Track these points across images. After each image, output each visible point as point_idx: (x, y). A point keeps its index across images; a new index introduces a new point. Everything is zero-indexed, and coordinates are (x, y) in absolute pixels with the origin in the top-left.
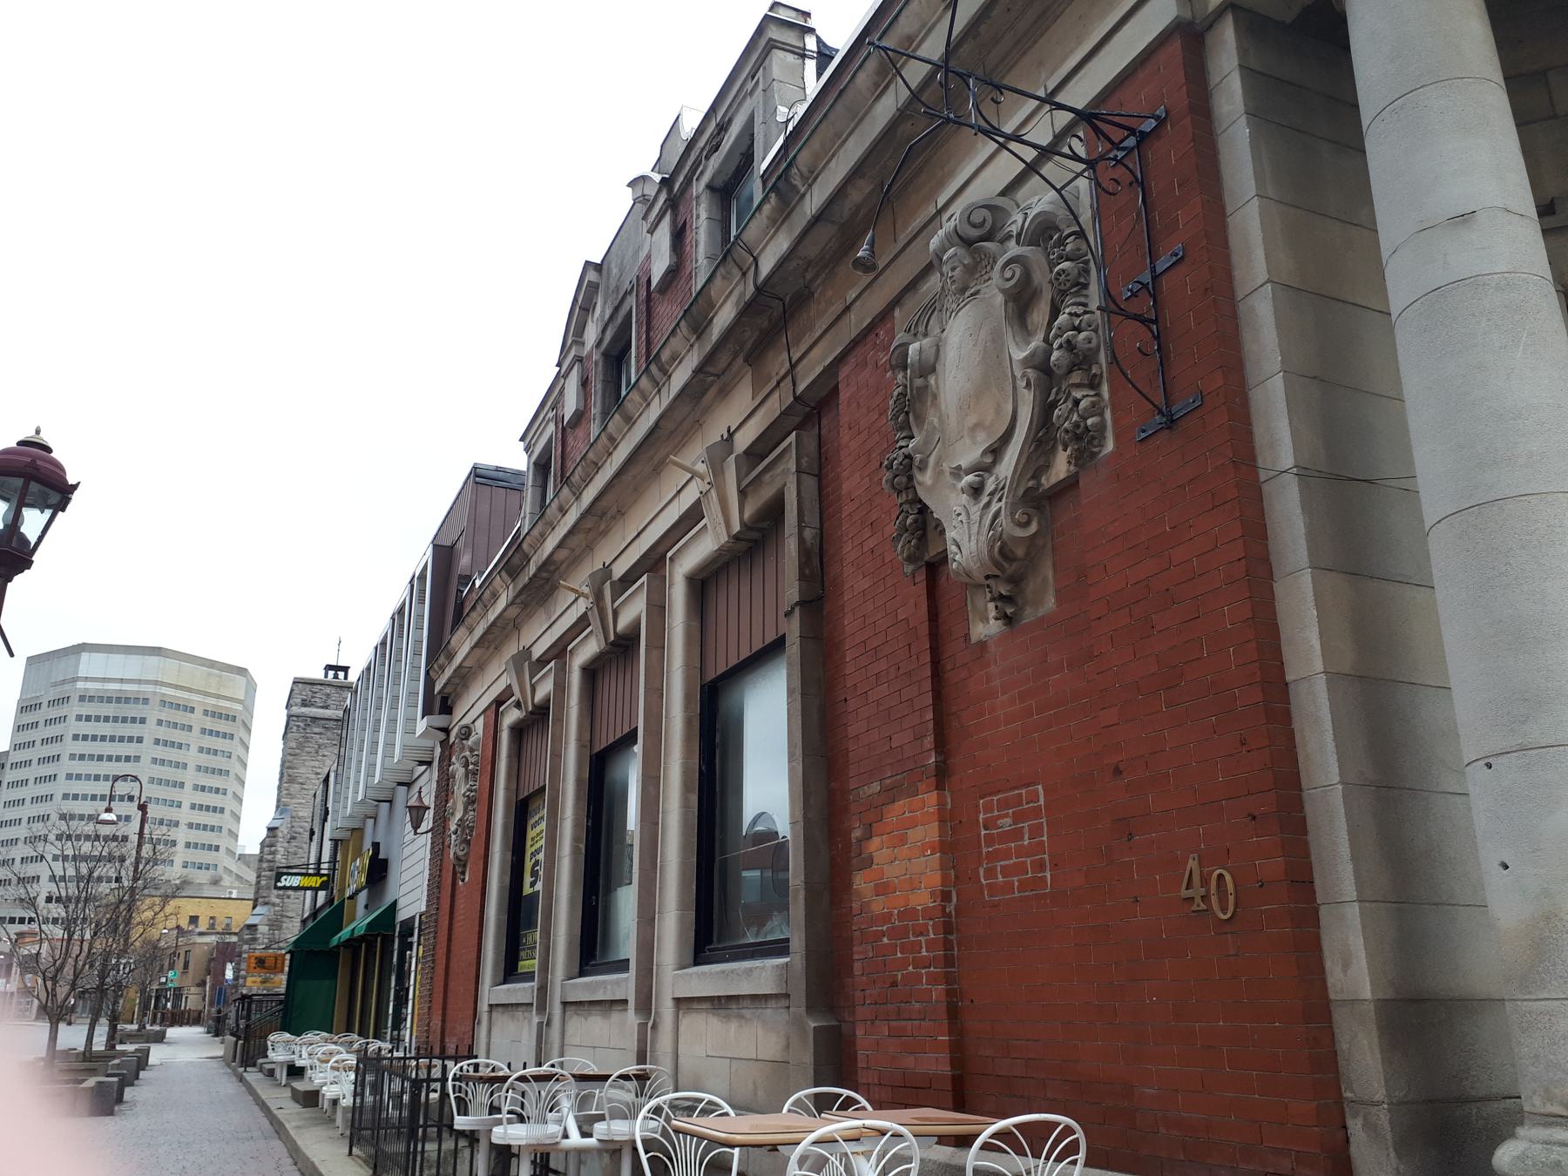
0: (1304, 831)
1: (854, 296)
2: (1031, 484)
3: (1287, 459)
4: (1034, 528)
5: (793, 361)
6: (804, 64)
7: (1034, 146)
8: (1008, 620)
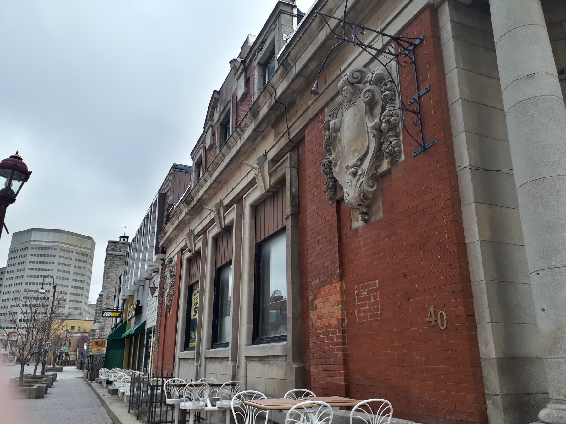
1: (311, 103)
2: (374, 172)
3: (466, 163)
4: (375, 187)
5: (289, 126)
6: (293, 19)
7: (376, 49)
8: (366, 221)
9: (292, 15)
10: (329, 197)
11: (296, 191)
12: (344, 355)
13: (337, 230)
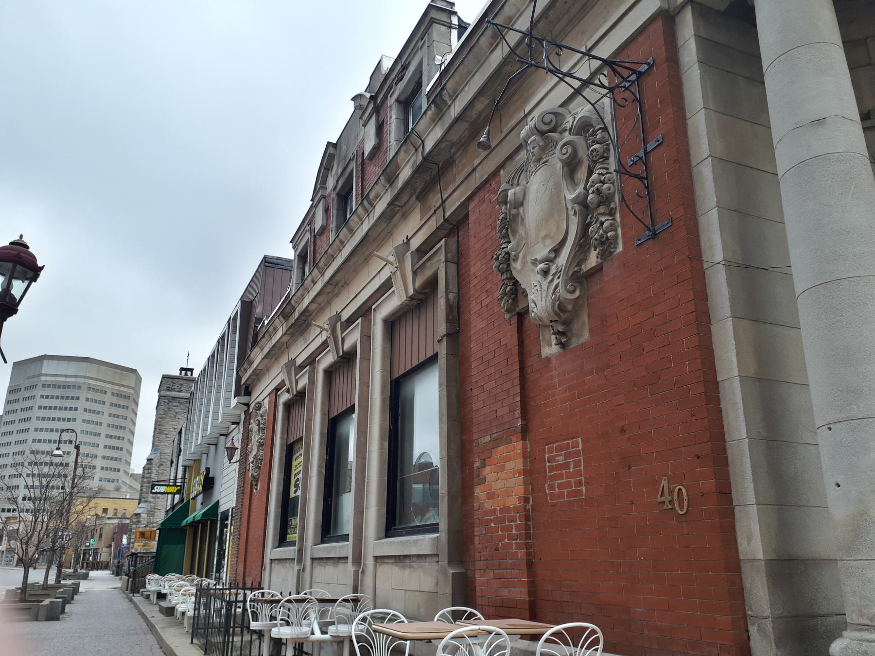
1: (478, 162)
2: (576, 269)
3: (719, 256)
4: (577, 294)
5: (444, 199)
6: (451, 32)
8: (562, 345)
9: (450, 27)
10: (505, 308)
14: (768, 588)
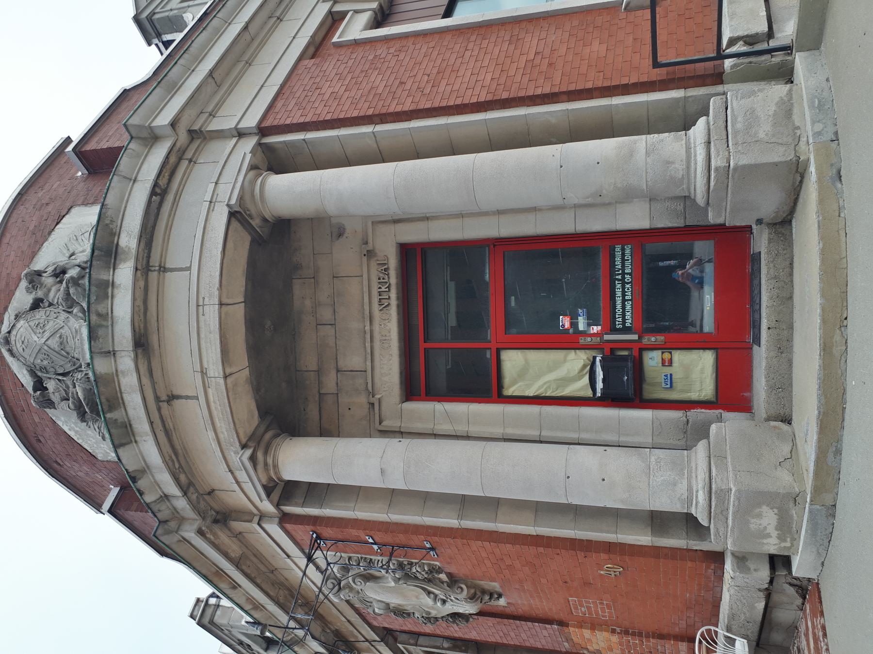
0: (591, 541)
1: (344, 619)
2: (445, 585)
3: (456, 522)
5: (364, 640)
6: (222, 606)
7: (307, 566)
8: (500, 596)
9: (218, 606)
11: (448, 642)
12: (653, 638)
13: (506, 620)
14: (669, 538)
